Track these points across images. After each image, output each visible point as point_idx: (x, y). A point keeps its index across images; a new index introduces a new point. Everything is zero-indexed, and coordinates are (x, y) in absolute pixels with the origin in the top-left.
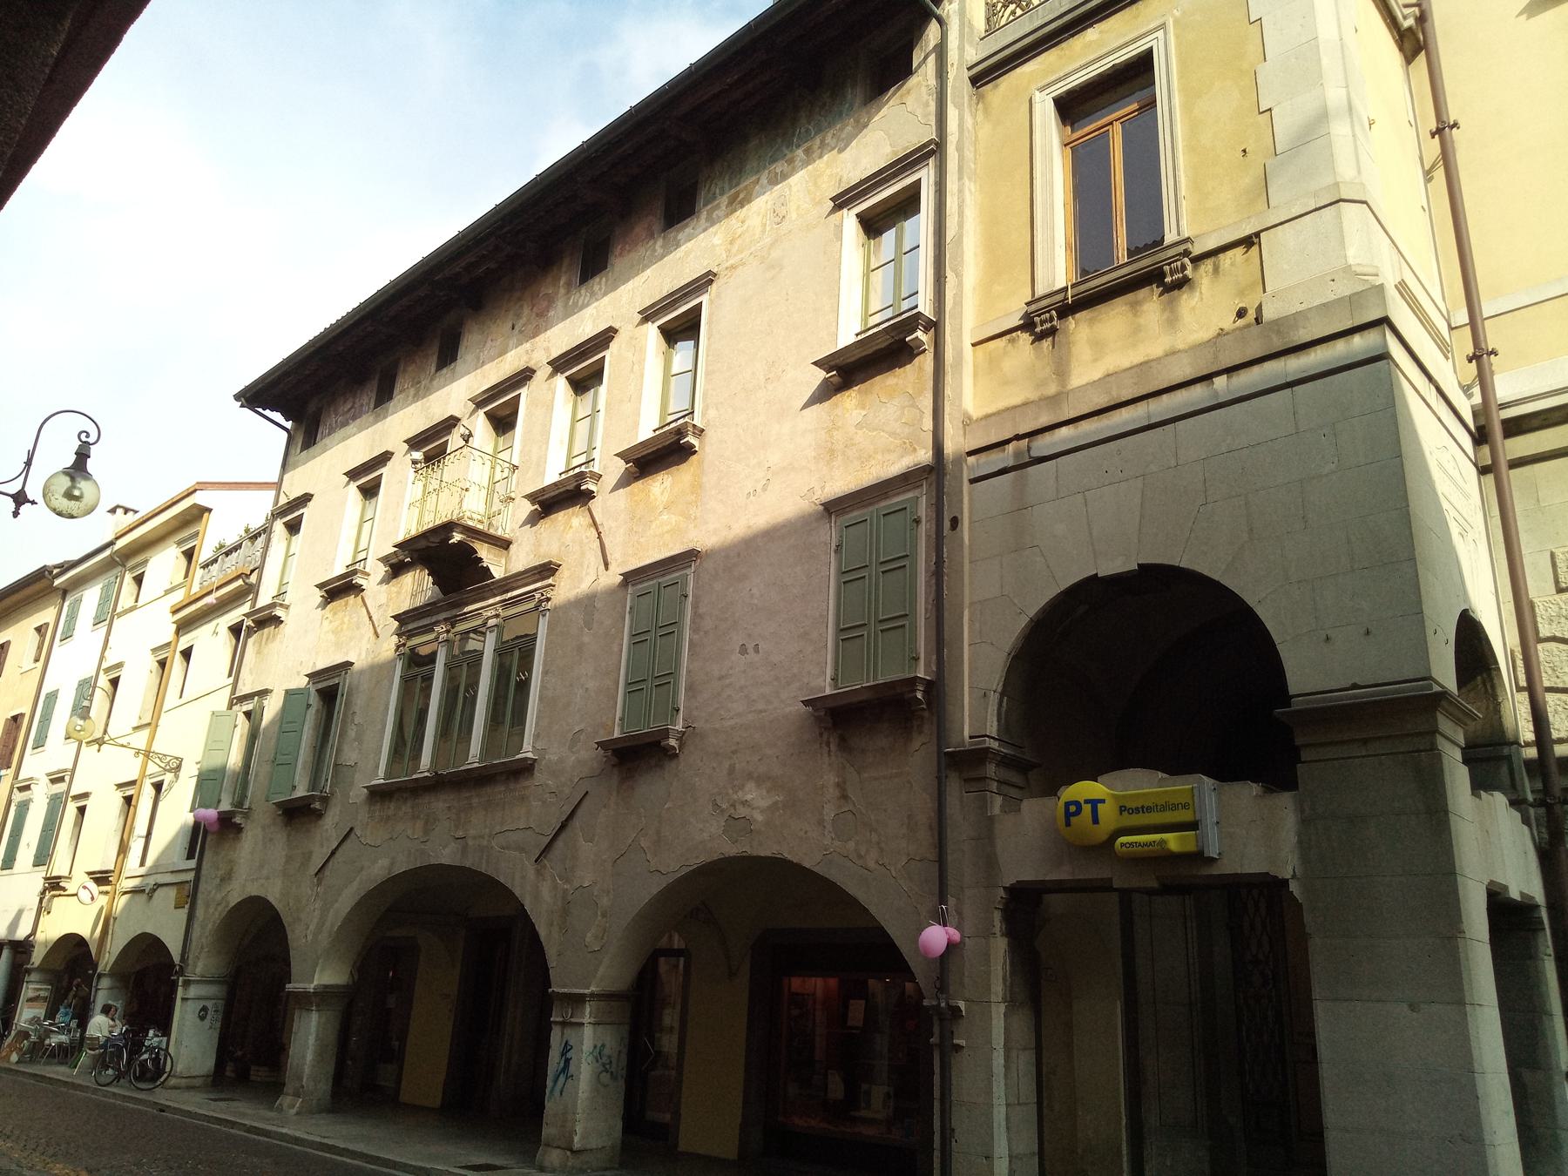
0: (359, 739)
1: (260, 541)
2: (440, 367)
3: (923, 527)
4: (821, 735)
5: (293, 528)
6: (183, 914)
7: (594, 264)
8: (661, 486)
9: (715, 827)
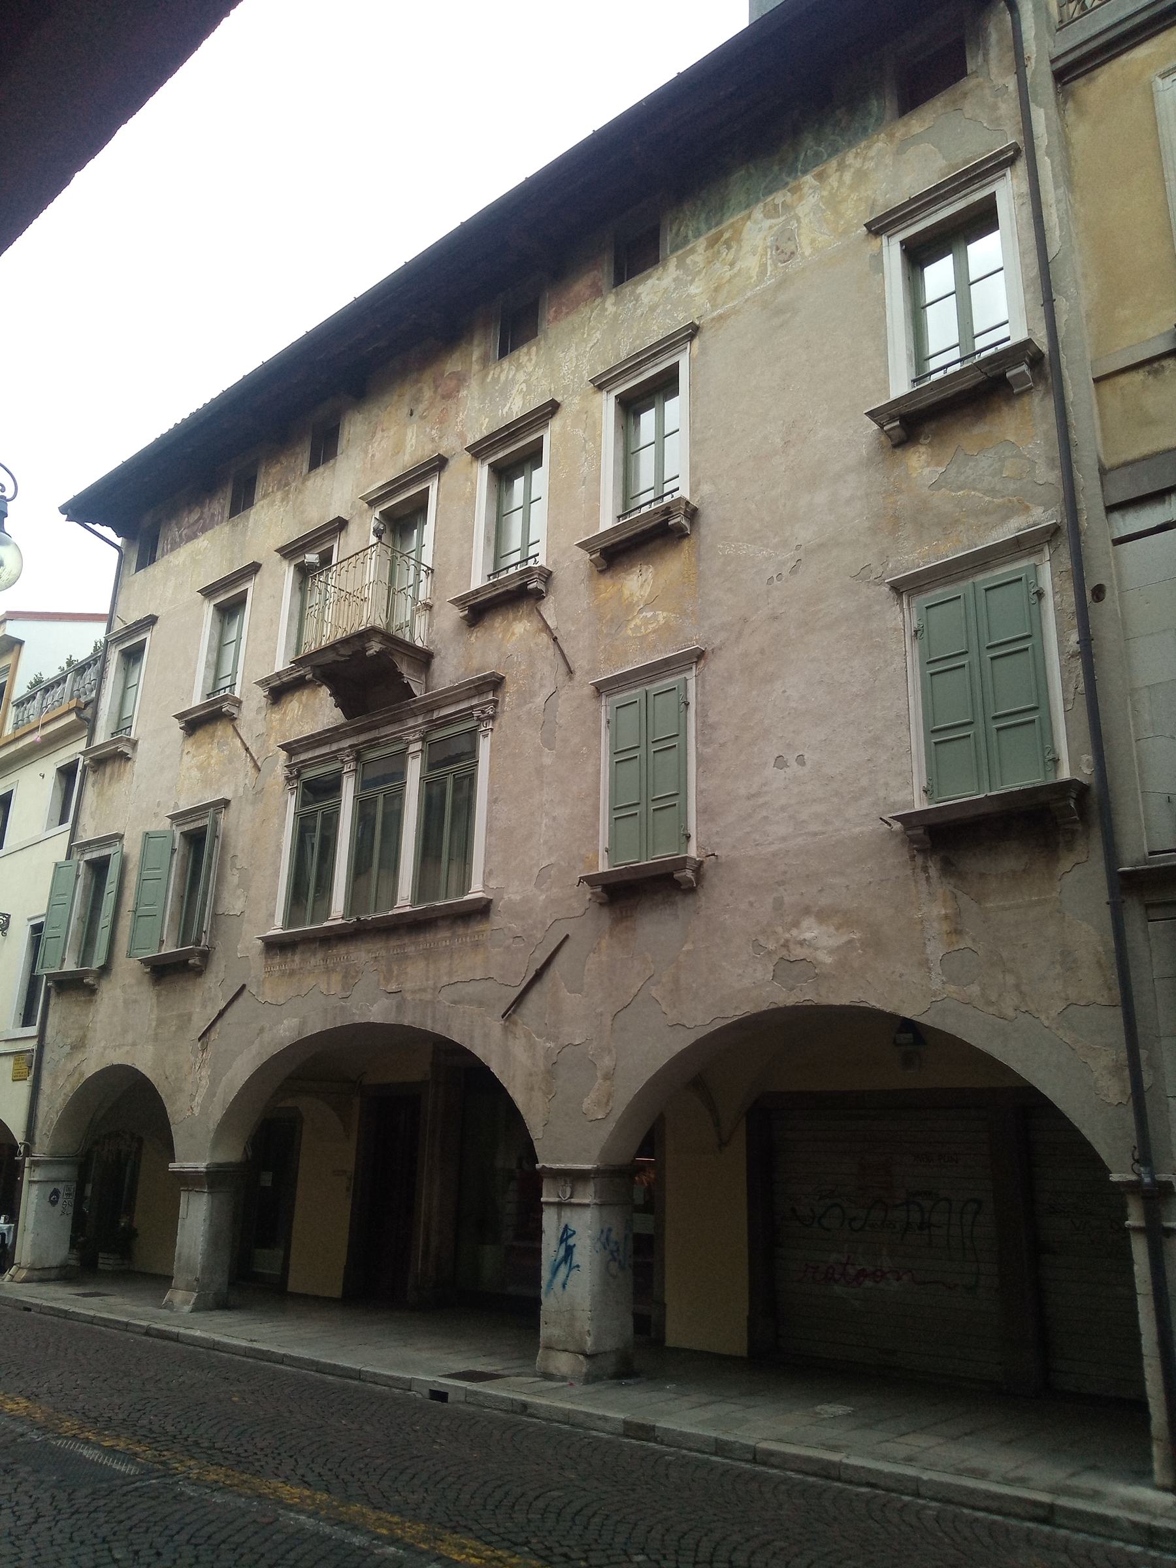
0: (244, 884)
1: (91, 674)
2: (314, 465)
3: (1049, 603)
4: (913, 858)
5: (133, 656)
6: (24, 1088)
7: (517, 329)
8: (638, 582)
9: (762, 972)
